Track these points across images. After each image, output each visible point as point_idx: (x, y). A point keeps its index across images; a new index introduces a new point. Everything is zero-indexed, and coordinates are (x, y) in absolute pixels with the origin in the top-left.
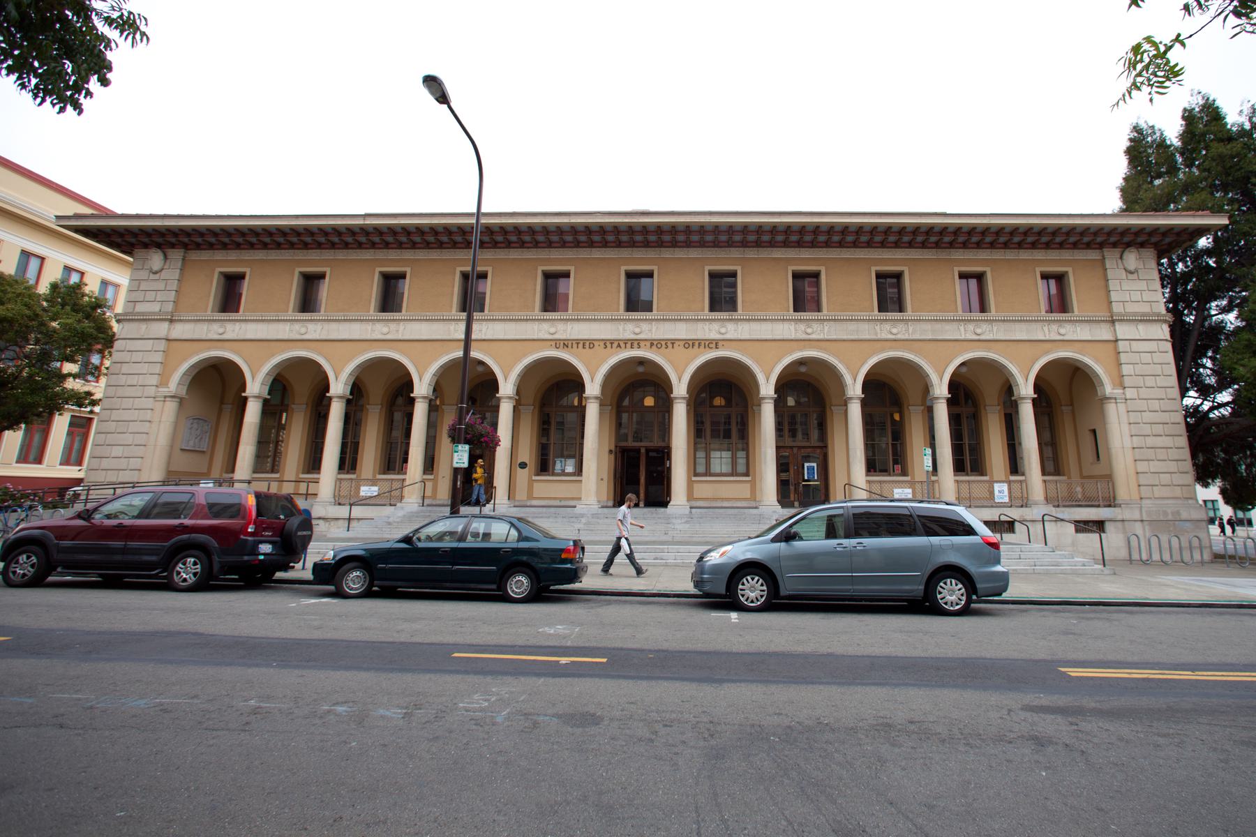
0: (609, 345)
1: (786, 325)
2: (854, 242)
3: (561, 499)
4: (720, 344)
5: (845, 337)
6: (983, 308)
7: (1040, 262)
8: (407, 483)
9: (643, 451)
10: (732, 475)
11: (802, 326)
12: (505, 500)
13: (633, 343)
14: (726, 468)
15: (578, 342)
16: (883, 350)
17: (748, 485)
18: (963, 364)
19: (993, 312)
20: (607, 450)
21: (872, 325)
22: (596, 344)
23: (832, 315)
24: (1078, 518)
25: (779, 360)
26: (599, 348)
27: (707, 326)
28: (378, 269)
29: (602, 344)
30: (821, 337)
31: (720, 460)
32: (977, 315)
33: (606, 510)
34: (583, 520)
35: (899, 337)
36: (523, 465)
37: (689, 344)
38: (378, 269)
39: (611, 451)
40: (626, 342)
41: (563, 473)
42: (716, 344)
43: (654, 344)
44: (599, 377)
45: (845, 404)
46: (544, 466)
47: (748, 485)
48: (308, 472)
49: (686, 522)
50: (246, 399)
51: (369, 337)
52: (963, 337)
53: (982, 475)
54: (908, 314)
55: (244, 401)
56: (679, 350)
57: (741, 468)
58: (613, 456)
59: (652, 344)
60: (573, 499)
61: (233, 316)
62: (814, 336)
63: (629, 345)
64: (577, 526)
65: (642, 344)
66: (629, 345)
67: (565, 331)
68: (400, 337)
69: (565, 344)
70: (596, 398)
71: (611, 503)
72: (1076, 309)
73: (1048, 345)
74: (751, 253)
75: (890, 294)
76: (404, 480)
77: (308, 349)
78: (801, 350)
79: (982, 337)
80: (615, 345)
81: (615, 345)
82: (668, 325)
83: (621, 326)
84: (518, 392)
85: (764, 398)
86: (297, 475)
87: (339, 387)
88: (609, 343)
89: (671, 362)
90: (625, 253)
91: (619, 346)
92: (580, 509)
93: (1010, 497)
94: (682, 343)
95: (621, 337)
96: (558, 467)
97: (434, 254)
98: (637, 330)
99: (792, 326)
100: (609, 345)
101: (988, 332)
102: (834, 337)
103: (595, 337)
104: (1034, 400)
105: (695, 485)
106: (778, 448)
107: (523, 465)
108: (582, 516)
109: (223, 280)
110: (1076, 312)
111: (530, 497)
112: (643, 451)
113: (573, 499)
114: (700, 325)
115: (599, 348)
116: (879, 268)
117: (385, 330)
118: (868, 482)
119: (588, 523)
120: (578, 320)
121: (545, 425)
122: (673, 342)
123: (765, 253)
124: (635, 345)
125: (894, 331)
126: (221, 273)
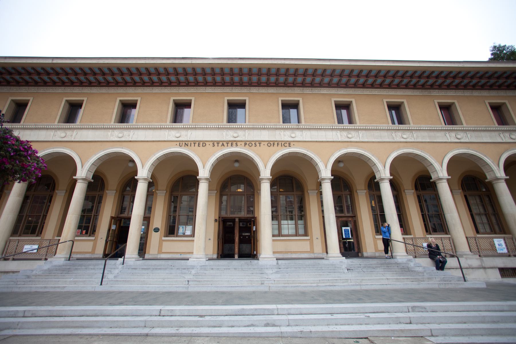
0: (216, 144)
1: (334, 132)
2: (320, 84)
3: (181, 253)
4: (292, 144)
5: (374, 140)
6: (401, 121)
7: (228, 94)
8: (60, 242)
9: (237, 220)
10: (296, 235)
11: (345, 133)
12: (135, 254)
13: (232, 143)
14: (292, 231)
15: (195, 142)
16: (399, 148)
17: (308, 242)
18: (338, 161)
19: (358, 124)
20: (213, 219)
21: (389, 133)
22: (207, 143)
23: (364, 126)
24: (502, 265)
25: (332, 154)
26: (209, 146)
27: (282, 132)
28: (65, 99)
29: (211, 143)
30: (358, 140)
31: (288, 226)
32: (397, 126)
33: (212, 262)
34: (193, 272)
35: (408, 140)
36: (157, 230)
37: (271, 143)
38: (385, 101)
39: (216, 220)
40: (228, 142)
41: (184, 235)
42: (289, 144)
43: (247, 143)
44: (149, 164)
45: (320, 184)
46: (171, 231)
47: (308, 242)
48: (167, 236)
49: (277, 272)
50: (75, 181)
51: (51, 139)
52: (449, 141)
53: (447, 234)
54: (412, 126)
55: (75, 182)
56: (264, 147)
57: (301, 231)
58: (217, 223)
59: (245, 144)
60: (189, 253)
61: (71, 125)
62: (353, 140)
63: (230, 144)
64: (188, 277)
65: (239, 144)
66: (230, 144)
67: (186, 135)
68: (73, 139)
69: (186, 144)
70: (207, 179)
71: (215, 256)
72: (411, 122)
73: (396, 145)
74: (307, 91)
75: (448, 113)
76: (59, 240)
77: (358, 147)
78: (346, 148)
79: (462, 141)
80: (221, 144)
81: (221, 144)
82: (256, 132)
83: (225, 132)
84: (153, 177)
85: (262, 179)
86: (54, 237)
87: (143, 173)
88: (216, 143)
89: (260, 156)
90: (227, 90)
91: (223, 145)
92: (191, 262)
93: (507, 249)
94: (266, 143)
95: (224, 139)
96: (181, 231)
97: (104, 90)
98: (235, 135)
99: (339, 133)
100: (216, 144)
101: (299, 136)
102: (366, 140)
103: (205, 138)
104: (448, 180)
105: (164, 243)
106: (337, 217)
107: (157, 230)
108: (193, 267)
109: (68, 105)
110: (465, 124)
111: (160, 252)
112: (237, 220)
113: (189, 253)
114: (278, 132)
115: (209, 146)
116: (122, 99)
117: (63, 135)
118: (404, 238)
119: (195, 275)
120: (195, 128)
121: (173, 201)
122: (260, 142)
123: (316, 91)
124: (234, 143)
125: (405, 136)
126: (67, 101)
